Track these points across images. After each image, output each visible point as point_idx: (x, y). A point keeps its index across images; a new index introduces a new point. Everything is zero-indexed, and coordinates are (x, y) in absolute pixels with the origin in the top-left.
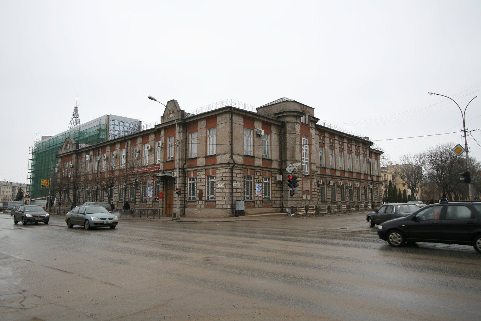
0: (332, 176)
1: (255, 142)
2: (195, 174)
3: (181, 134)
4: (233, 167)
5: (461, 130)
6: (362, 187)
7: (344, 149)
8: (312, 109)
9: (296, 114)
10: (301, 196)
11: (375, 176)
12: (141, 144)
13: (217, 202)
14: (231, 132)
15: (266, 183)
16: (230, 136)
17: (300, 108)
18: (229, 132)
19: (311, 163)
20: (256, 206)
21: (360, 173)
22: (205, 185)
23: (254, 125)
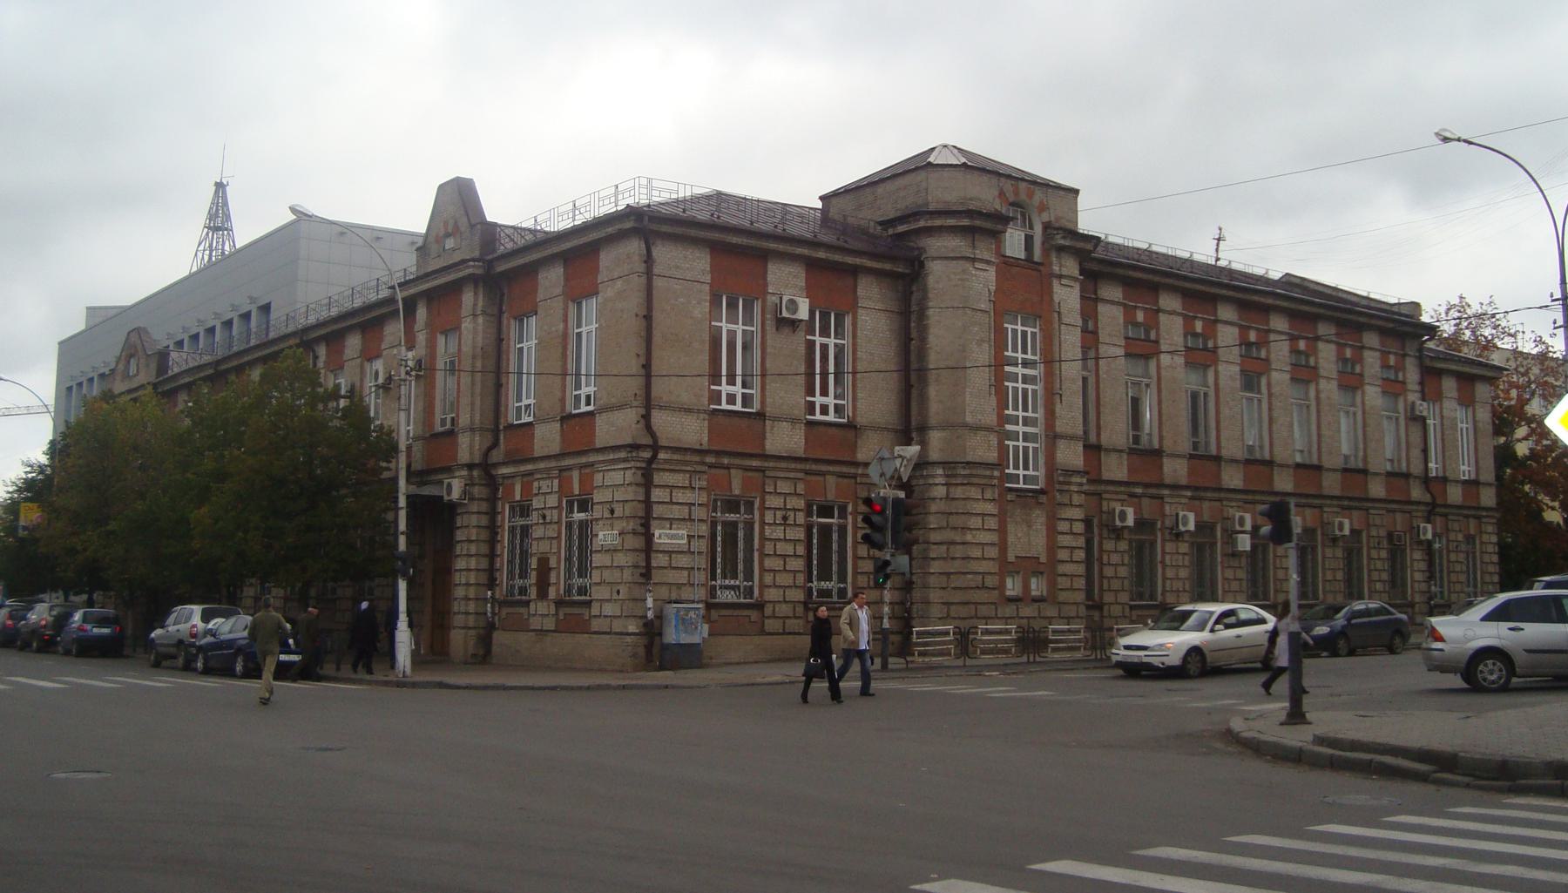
0: (1197, 489)
1: (769, 350)
2: (526, 489)
3: (480, 320)
4: (651, 461)
5: (1552, 296)
6: (1374, 533)
7: (1270, 365)
8: (1062, 193)
9: (966, 222)
10: (990, 581)
11: (1457, 482)
12: (359, 360)
13: (595, 610)
14: (644, 316)
15: (829, 526)
16: (643, 334)
17: (997, 193)
18: (637, 315)
19: (1053, 437)
20: (771, 625)
21: (1364, 472)
22: (559, 537)
23: (764, 277)
